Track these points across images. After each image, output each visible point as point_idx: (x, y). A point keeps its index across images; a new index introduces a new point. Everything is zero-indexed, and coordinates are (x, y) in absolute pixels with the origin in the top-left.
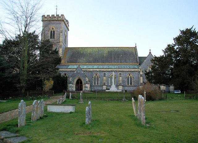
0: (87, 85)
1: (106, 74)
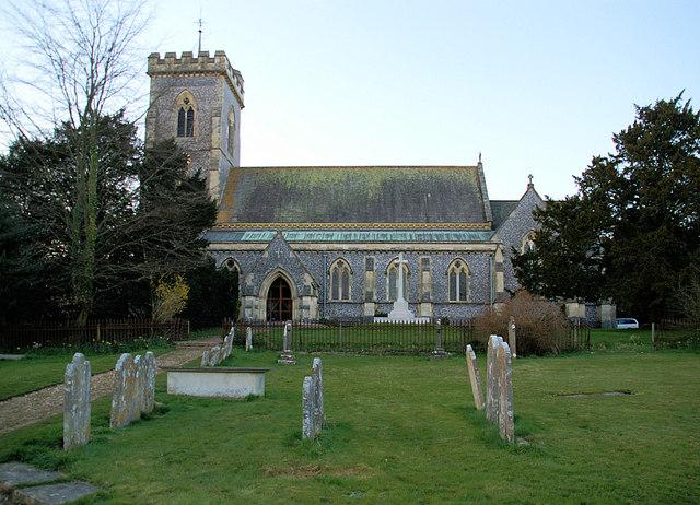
0: (307, 301)
1: (376, 261)
